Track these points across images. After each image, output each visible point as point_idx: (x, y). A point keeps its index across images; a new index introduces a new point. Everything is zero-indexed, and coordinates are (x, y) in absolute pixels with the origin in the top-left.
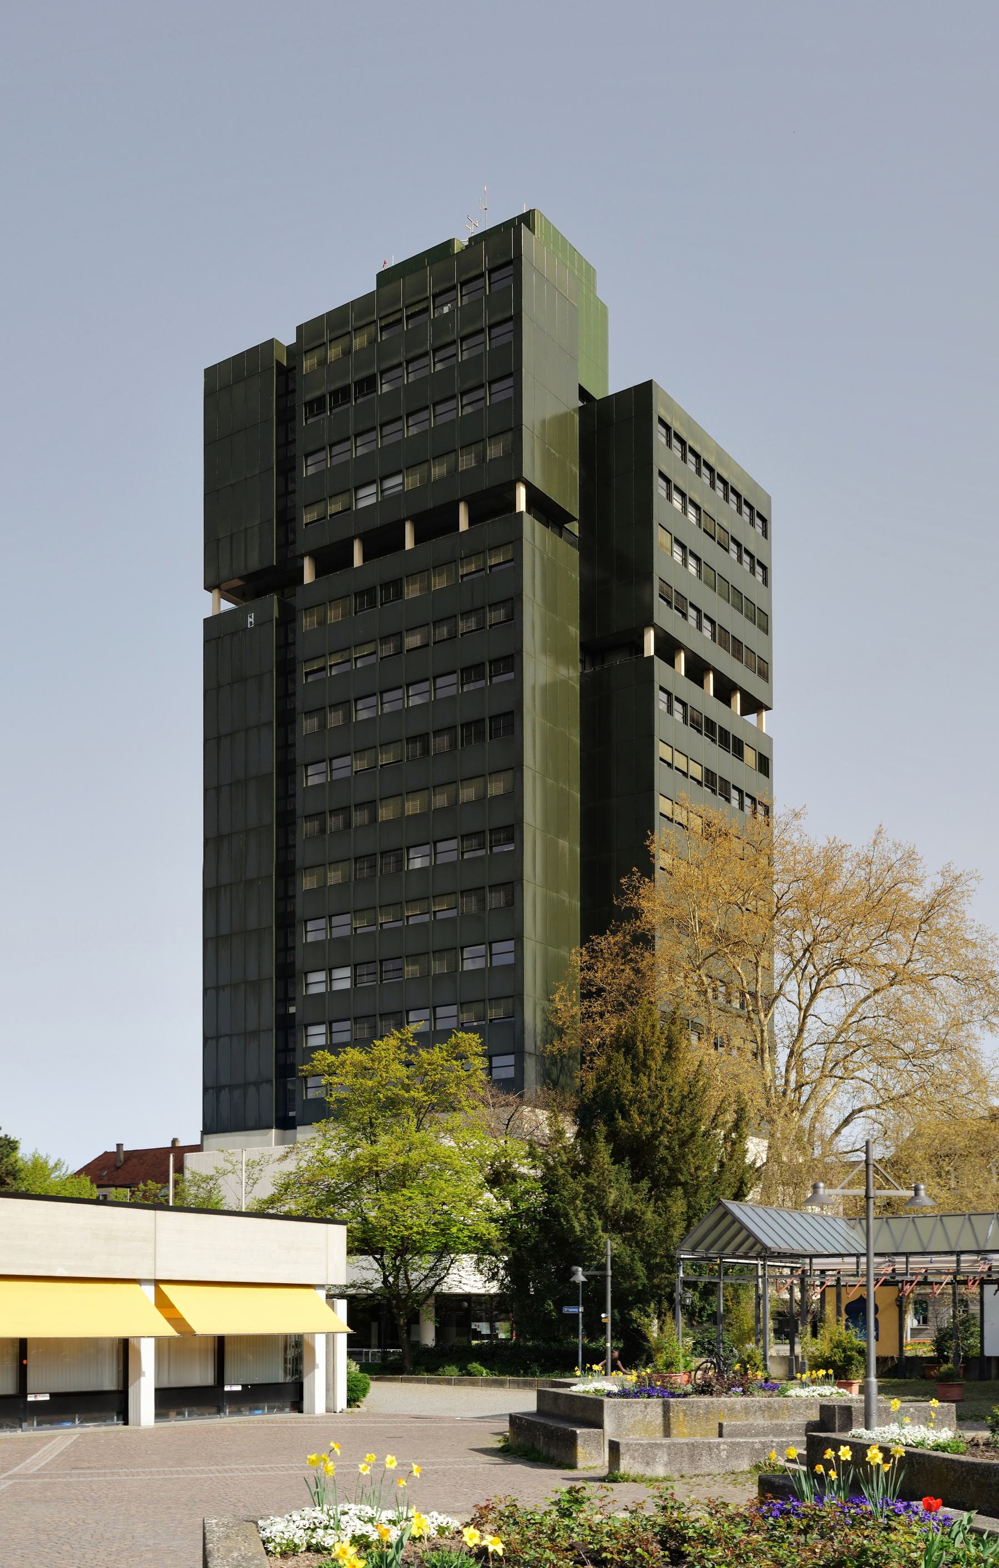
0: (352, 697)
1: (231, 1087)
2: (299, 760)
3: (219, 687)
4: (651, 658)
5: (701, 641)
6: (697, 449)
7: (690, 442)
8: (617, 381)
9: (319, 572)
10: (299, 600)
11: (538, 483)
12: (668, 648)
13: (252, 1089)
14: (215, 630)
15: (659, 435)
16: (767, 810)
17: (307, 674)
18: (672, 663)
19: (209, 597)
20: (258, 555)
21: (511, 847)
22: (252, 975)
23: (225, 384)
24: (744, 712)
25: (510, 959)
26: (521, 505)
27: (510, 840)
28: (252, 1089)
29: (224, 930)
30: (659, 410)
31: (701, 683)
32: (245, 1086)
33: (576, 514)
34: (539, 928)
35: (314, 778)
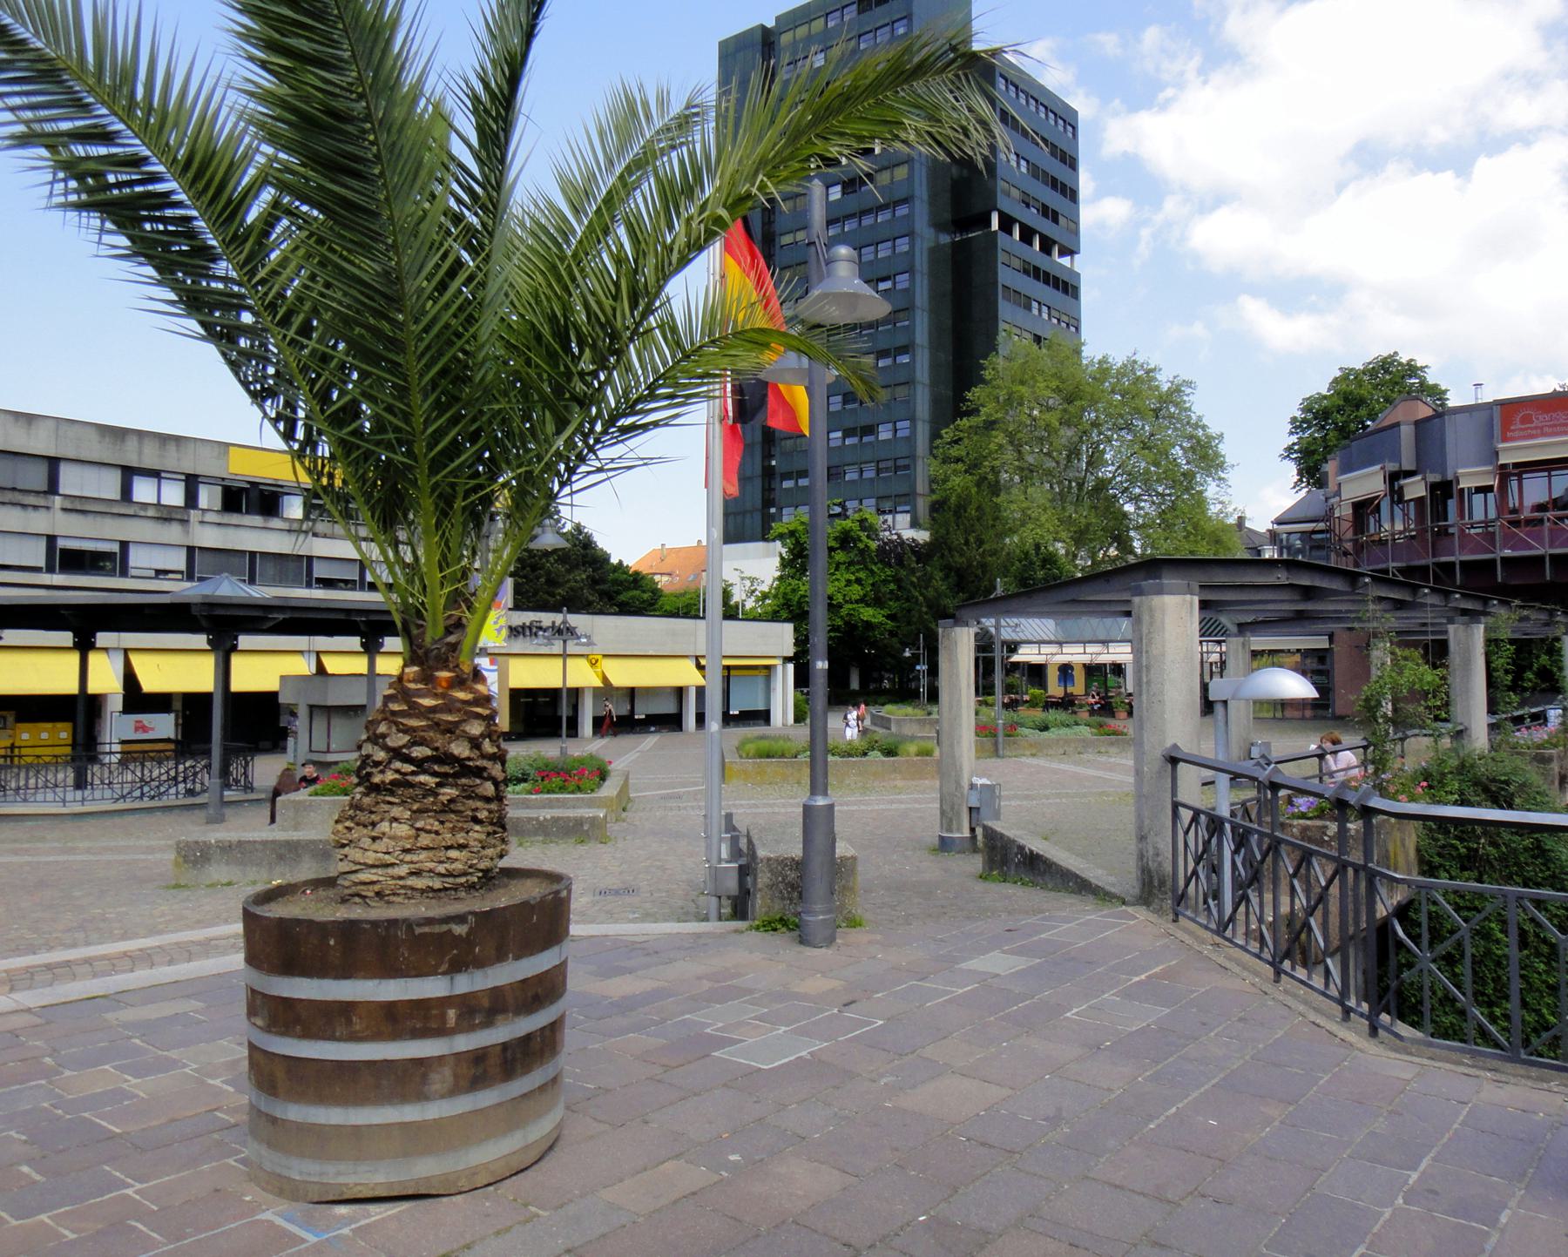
1: (735, 514)
5: (1032, 217)
31: (1030, 244)
32: (744, 513)
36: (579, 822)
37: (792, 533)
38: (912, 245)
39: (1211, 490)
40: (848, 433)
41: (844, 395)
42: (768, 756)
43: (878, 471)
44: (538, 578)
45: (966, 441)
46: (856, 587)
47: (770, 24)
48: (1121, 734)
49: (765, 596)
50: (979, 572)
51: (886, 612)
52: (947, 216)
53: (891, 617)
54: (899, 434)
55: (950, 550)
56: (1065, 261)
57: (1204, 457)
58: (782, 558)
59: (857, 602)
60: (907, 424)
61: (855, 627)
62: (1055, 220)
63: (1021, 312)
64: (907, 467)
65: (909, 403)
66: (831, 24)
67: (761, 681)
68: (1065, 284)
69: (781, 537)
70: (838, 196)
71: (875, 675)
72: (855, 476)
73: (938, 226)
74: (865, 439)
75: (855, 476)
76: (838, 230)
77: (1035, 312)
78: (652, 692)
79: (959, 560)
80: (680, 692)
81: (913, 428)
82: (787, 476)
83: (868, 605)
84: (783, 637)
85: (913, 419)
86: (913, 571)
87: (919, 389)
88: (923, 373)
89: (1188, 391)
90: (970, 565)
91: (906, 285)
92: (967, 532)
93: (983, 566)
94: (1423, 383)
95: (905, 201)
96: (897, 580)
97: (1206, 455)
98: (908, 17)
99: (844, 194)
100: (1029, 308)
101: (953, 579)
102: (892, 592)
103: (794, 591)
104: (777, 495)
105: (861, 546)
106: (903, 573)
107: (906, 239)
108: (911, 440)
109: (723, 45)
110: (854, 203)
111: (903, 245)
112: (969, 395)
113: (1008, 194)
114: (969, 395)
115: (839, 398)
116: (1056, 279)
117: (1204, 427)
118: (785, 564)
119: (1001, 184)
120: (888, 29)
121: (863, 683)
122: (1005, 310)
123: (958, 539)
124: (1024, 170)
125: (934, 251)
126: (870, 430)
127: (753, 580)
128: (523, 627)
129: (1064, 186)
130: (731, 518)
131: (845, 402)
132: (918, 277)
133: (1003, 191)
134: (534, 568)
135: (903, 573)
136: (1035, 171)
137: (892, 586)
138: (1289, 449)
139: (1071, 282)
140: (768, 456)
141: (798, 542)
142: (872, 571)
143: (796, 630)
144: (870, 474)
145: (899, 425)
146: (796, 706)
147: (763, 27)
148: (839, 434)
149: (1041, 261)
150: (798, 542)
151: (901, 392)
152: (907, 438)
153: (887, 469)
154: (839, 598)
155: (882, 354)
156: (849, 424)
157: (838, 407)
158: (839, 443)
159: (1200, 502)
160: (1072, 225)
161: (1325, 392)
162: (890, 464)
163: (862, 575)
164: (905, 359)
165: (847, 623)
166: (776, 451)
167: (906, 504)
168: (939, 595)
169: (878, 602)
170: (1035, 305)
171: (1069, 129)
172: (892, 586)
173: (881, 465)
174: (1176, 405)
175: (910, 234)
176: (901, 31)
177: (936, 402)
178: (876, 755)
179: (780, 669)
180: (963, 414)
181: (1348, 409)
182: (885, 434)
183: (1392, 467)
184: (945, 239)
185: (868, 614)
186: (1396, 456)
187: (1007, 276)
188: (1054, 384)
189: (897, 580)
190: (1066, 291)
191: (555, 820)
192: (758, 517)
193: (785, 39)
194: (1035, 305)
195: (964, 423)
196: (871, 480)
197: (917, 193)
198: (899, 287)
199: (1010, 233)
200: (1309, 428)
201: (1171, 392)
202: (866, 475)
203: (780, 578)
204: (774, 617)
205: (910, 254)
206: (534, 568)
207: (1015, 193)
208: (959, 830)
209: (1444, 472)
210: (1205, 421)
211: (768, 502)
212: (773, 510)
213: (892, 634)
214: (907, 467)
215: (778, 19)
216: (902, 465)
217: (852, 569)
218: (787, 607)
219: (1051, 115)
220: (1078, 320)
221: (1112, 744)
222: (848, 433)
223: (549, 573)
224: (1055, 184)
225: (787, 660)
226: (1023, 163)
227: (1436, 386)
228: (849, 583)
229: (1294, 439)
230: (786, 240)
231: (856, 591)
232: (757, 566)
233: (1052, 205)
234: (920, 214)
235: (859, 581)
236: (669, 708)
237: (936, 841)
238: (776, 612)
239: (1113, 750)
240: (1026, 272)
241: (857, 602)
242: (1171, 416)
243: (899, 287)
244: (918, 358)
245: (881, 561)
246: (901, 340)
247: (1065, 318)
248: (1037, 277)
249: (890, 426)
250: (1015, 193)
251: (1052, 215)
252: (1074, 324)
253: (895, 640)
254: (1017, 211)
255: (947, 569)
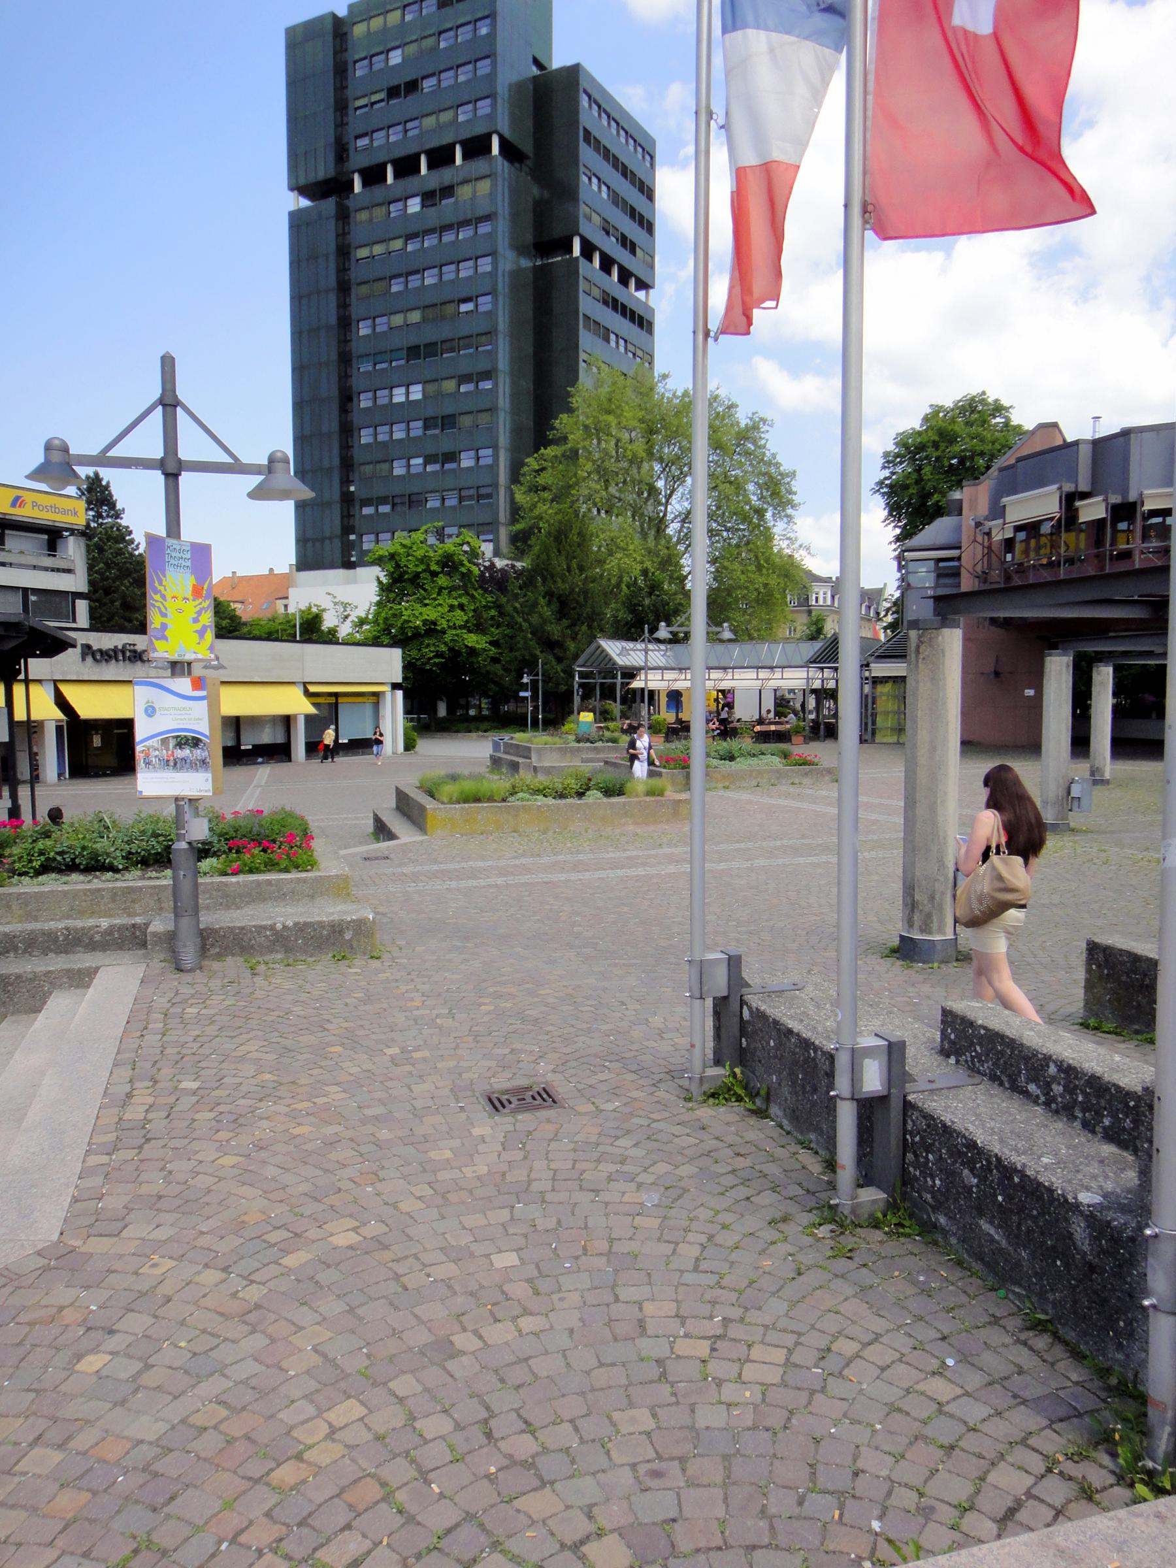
0: (388, 275)
1: (314, 541)
2: (354, 316)
3: (302, 402)
4: (577, 258)
5: (610, 246)
6: (608, 109)
7: (603, 105)
8: (559, 60)
9: (365, 184)
10: (351, 203)
11: (507, 134)
12: (588, 249)
13: (327, 542)
14: (297, 221)
15: (584, 101)
16: (652, 157)
17: (356, 109)
18: (591, 261)
19: (293, 195)
20: (323, 169)
21: (489, 347)
22: (326, 464)
23: (299, 40)
24: (638, 289)
25: (489, 461)
26: (495, 150)
27: (489, 378)
28: (327, 542)
29: (307, 432)
30: (583, 84)
31: (609, 273)
32: (323, 540)
33: (531, 155)
34: (507, 400)
35: (364, 330)
36: (337, 929)
37: (392, 556)
38: (495, 265)
39: (778, 528)
40: (429, 459)
41: (426, 420)
42: (477, 800)
43: (461, 499)
44: (112, 602)
45: (550, 470)
46: (459, 612)
47: (342, 12)
48: (811, 763)
49: (362, 622)
50: (581, 599)
51: (488, 638)
52: (529, 238)
53: (494, 643)
54: (482, 462)
55: (552, 576)
56: (641, 295)
57: (775, 494)
58: (380, 582)
59: (461, 627)
60: (489, 452)
61: (458, 653)
62: (633, 251)
63: (600, 342)
64: (489, 496)
65: (491, 430)
66: (408, 18)
67: (369, 710)
68: (641, 318)
69: (379, 561)
70: (417, 208)
71: (462, 702)
72: (437, 504)
73: (520, 250)
74: (447, 466)
75: (437, 504)
76: (418, 246)
77: (613, 344)
78: (256, 721)
79: (561, 586)
80: (287, 721)
81: (496, 457)
82: (366, 502)
83: (470, 631)
84: (388, 664)
85: (495, 447)
86: (516, 597)
87: (502, 415)
88: (504, 402)
89: (766, 428)
90: (572, 591)
91: (488, 307)
92: (569, 558)
93: (585, 592)
94: (1007, 424)
95: (487, 218)
96: (499, 607)
97: (777, 491)
98: (492, 16)
99: (423, 206)
100: (607, 340)
101: (555, 605)
102: (492, 618)
103: (394, 615)
104: (357, 522)
105: (463, 570)
106: (503, 600)
107: (489, 259)
108: (493, 468)
109: (291, 32)
110: (434, 216)
111: (485, 265)
112: (557, 423)
113: (590, 220)
114: (557, 423)
115: (420, 424)
116: (633, 313)
117: (777, 465)
118: (384, 589)
119: (583, 209)
120: (469, 27)
121: (450, 710)
122: (586, 339)
123: (559, 563)
124: (604, 195)
125: (516, 274)
126: (452, 457)
127: (345, 605)
128: (115, 650)
129: (641, 217)
130: (309, 545)
131: (426, 427)
132: (501, 299)
133: (585, 216)
134: (107, 591)
135: (503, 600)
136: (616, 199)
137: (493, 612)
138: (881, 483)
139: (646, 317)
140: (346, 481)
141: (398, 566)
142: (473, 596)
143: (404, 653)
144: (452, 502)
145: (482, 452)
146: (405, 734)
147: (334, 16)
148: (420, 461)
149: (617, 291)
150: (398, 566)
151: (483, 418)
152: (490, 467)
153: (470, 498)
154: (443, 624)
155: (464, 379)
156: (430, 449)
157: (420, 432)
158: (421, 469)
159: (768, 537)
160: (648, 258)
161: (918, 428)
162: (472, 492)
163: (464, 600)
164: (487, 385)
165: (451, 649)
166: (356, 476)
167: (489, 532)
168: (545, 621)
169: (478, 627)
170: (613, 337)
171: (648, 158)
172: (493, 612)
173: (463, 493)
174: (755, 443)
175: (493, 254)
176: (484, 31)
177: (517, 431)
178: (594, 796)
179: (388, 696)
180: (547, 443)
181: (943, 446)
182: (467, 461)
183: (1069, 487)
184: (526, 263)
185: (473, 640)
186: (1073, 476)
187: (587, 305)
188: (641, 414)
189: (499, 607)
190: (641, 325)
191: (300, 928)
192: (337, 543)
193: (359, 30)
194: (613, 337)
195: (550, 451)
196: (453, 508)
197: (500, 211)
198: (481, 309)
199: (590, 260)
200: (901, 463)
201: (747, 429)
202: (448, 503)
203: (379, 604)
204: (375, 642)
205: (493, 274)
206: (107, 591)
207: (596, 219)
208: (941, 930)
209: (1125, 491)
210: (779, 459)
211: (347, 529)
212: (352, 537)
213: (495, 660)
214: (489, 496)
215: (350, 7)
216: (484, 494)
217: (454, 594)
218: (383, 632)
219: (631, 141)
220: (652, 356)
221: (806, 774)
222: (429, 459)
223: (124, 597)
224: (633, 213)
225: (395, 686)
226: (604, 188)
227: (1019, 426)
228: (452, 608)
229: (887, 473)
230: (363, 253)
231: (459, 617)
232: (353, 593)
233: (630, 236)
234: (502, 229)
235: (461, 607)
236: (267, 737)
237: (896, 942)
238: (376, 638)
239: (806, 781)
240: (605, 303)
241: (461, 627)
242: (748, 453)
243: (481, 309)
244: (501, 385)
245: (481, 587)
246: (483, 366)
247: (639, 353)
248: (615, 309)
249: (472, 453)
250: (596, 219)
251: (630, 246)
252: (649, 357)
253: (498, 666)
254: (597, 238)
255: (549, 595)
